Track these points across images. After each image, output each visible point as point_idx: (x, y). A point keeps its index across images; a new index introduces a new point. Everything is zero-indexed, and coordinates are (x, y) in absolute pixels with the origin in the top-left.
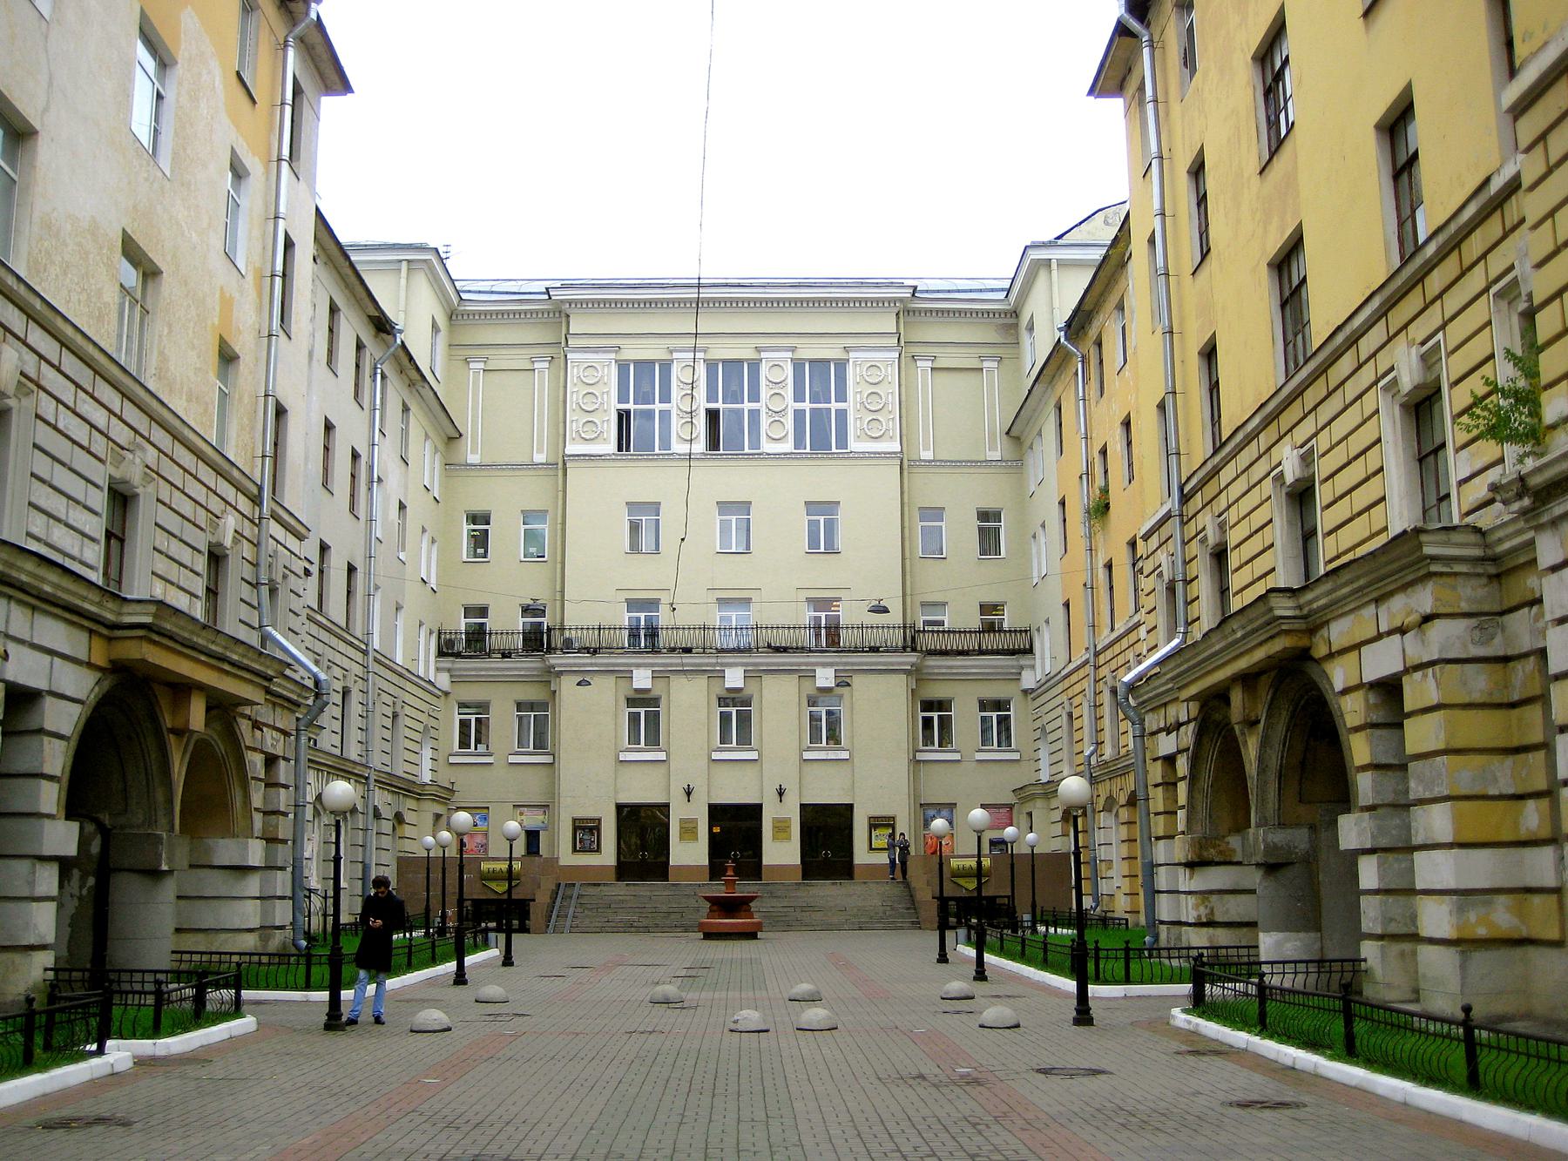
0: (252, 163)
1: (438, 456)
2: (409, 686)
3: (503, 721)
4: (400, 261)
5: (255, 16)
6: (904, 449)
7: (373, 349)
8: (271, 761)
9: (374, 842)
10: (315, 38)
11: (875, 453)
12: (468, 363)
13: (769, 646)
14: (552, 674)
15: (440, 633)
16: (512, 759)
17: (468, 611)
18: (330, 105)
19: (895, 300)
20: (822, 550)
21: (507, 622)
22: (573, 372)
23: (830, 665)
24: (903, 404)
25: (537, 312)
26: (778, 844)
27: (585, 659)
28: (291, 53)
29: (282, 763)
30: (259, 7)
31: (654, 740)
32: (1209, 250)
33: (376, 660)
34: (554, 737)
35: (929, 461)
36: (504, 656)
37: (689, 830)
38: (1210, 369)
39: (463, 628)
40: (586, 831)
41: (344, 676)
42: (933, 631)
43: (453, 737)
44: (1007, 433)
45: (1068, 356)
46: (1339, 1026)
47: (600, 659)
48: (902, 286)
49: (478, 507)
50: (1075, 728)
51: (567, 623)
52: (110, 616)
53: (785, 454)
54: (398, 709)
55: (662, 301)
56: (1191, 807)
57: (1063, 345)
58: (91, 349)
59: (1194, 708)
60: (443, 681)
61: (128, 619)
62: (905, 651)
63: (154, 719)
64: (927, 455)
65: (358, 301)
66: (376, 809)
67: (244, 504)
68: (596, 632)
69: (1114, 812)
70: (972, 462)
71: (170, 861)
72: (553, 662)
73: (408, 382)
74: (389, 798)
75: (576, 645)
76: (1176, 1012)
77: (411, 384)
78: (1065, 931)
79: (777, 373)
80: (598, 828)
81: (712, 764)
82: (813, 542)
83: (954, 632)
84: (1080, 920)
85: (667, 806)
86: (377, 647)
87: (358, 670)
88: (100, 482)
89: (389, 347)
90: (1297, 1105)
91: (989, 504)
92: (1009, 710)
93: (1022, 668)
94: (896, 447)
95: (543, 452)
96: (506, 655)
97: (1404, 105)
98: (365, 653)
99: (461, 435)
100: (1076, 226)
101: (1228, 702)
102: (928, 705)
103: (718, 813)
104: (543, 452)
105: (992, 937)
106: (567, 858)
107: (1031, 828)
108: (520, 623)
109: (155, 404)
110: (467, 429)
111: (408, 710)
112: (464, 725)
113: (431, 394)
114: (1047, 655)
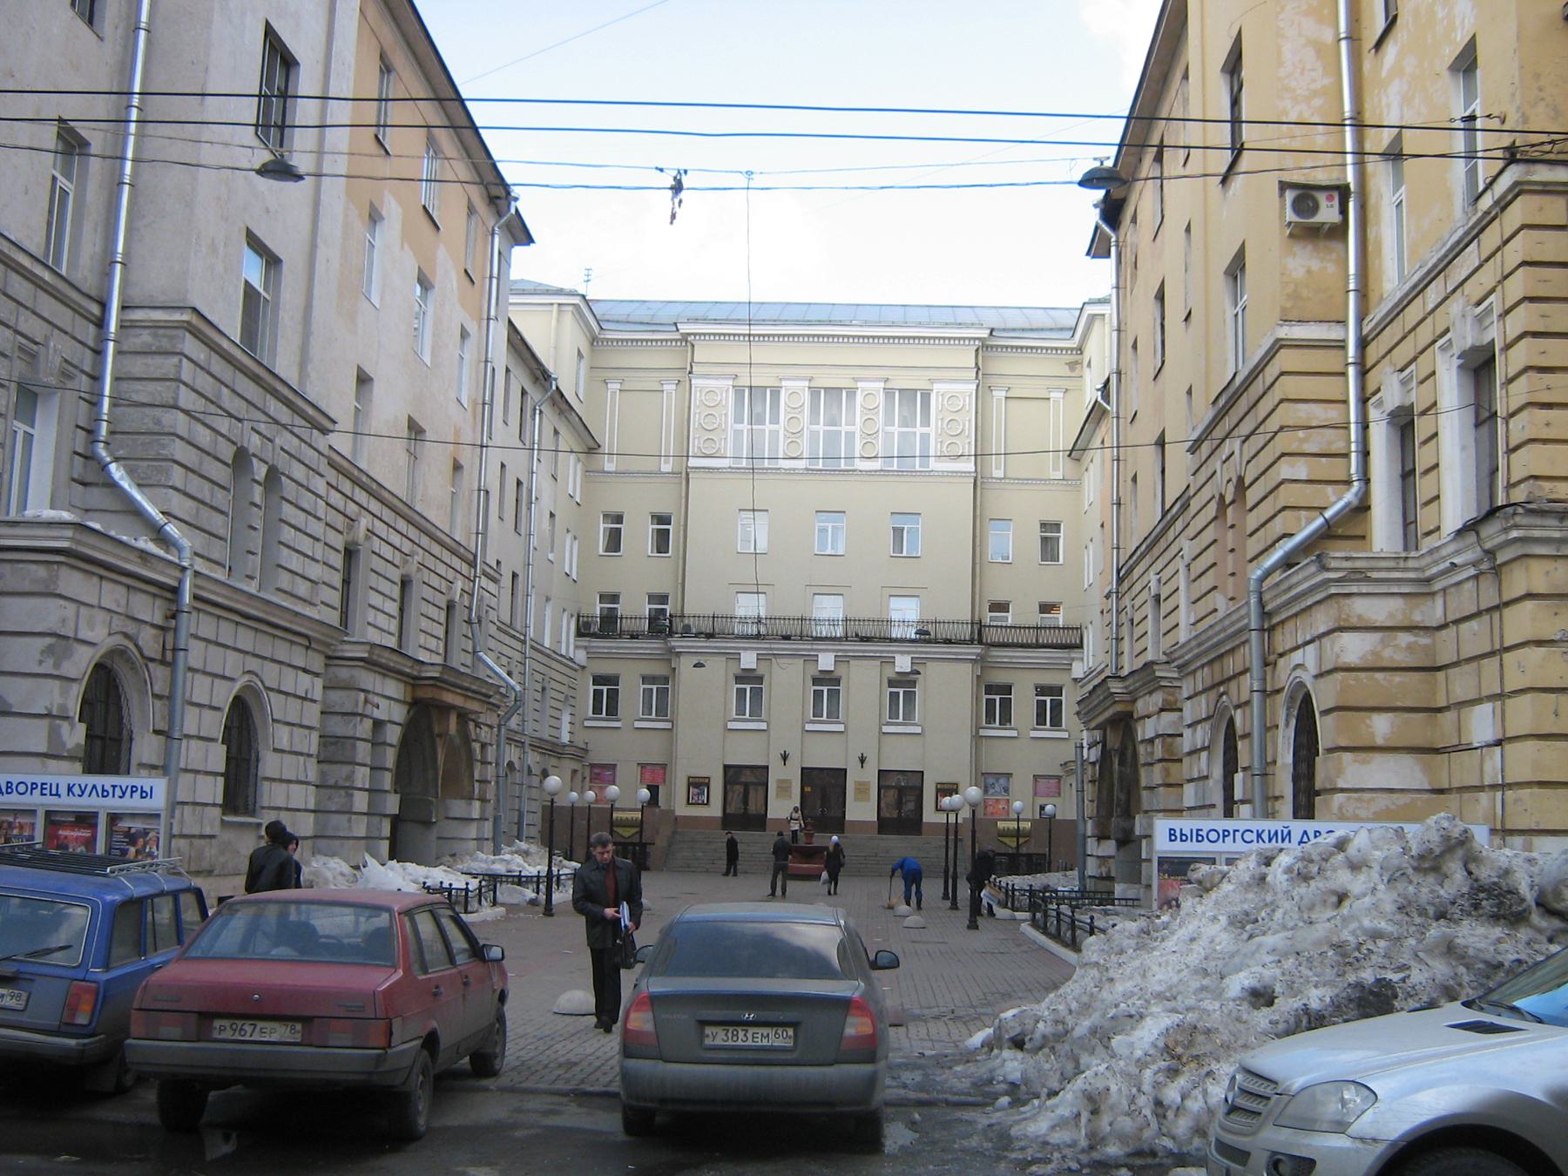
0: (472, 328)
1: (579, 466)
2: (554, 665)
3: (632, 693)
4: (552, 304)
5: (474, 218)
6: (979, 470)
7: (534, 394)
8: (484, 746)
9: (526, 794)
10: (516, 223)
11: (952, 472)
13: (857, 635)
14: (672, 654)
15: (579, 616)
16: (638, 724)
17: (603, 598)
18: (518, 252)
20: (904, 554)
21: (635, 607)
23: (908, 653)
27: (702, 643)
28: (497, 239)
29: (489, 748)
30: (477, 212)
31: (756, 712)
33: (532, 647)
34: (673, 706)
35: (1000, 479)
36: (632, 637)
39: (598, 613)
40: (698, 784)
41: (509, 663)
43: (588, 706)
45: (1104, 412)
47: (712, 643)
51: (686, 612)
52: (415, 673)
53: (876, 471)
54: (546, 685)
57: (1100, 403)
58: (396, 502)
60: (581, 656)
61: (424, 675)
62: (972, 644)
63: (430, 728)
65: (524, 361)
66: (529, 767)
67: (465, 568)
70: (1041, 480)
71: (436, 816)
72: (673, 644)
73: (558, 411)
74: (538, 758)
75: (694, 631)
77: (561, 412)
80: (708, 786)
81: (805, 734)
85: (767, 767)
86: (532, 635)
87: (517, 656)
89: (547, 391)
93: (1073, 659)
98: (524, 642)
102: (990, 689)
103: (807, 774)
106: (682, 810)
108: (646, 609)
109: (423, 522)
110: (607, 441)
111: (554, 685)
112: (598, 694)
113: (577, 419)
114: (1091, 653)
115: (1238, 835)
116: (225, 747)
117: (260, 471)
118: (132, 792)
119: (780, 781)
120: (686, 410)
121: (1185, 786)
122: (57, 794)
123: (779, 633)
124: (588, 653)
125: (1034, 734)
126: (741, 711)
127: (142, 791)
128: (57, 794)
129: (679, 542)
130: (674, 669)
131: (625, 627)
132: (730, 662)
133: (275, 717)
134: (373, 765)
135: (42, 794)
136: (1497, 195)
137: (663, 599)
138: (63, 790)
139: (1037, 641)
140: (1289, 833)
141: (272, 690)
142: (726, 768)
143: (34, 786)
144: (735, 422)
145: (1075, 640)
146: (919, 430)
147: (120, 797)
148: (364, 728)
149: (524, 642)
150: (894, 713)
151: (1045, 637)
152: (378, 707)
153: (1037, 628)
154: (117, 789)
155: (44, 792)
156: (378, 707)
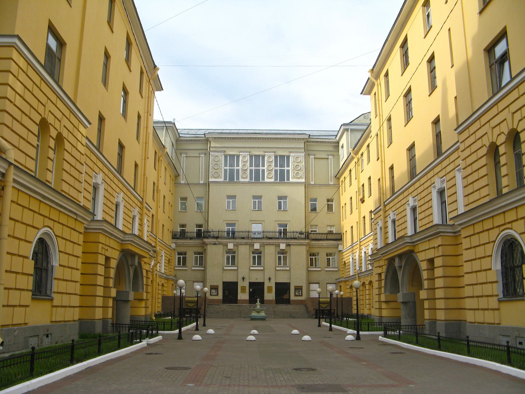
3: (191, 258)
6: (306, 182)
8: (147, 271)
12: (181, 154)
13: (267, 237)
15: (173, 232)
16: (193, 268)
19: (304, 139)
21: (192, 229)
22: (211, 158)
24: (306, 168)
25: (203, 140)
26: (269, 294)
27: (214, 240)
31: (259, 264)
32: (392, 142)
35: (313, 185)
37: (243, 289)
39: (179, 231)
42: (313, 234)
44: (336, 177)
46: (415, 338)
47: (220, 240)
48: (305, 134)
49: (184, 196)
55: (237, 138)
56: (385, 287)
59: (386, 262)
64: (312, 183)
68: (218, 233)
72: (205, 241)
76: (380, 337)
79: (269, 158)
82: (280, 207)
83: (319, 234)
84: (357, 316)
85: (237, 282)
88: (114, 203)
90: (405, 353)
94: (303, 180)
95: (202, 180)
96: (191, 238)
97: (437, 119)
99: (179, 175)
100: (356, 119)
101: (394, 261)
103: (251, 284)
104: (202, 180)
105: (333, 320)
107: (341, 290)
108: (195, 229)
112: (179, 258)
116: (33, 262)
117: (54, 133)
119: (242, 287)
120: (208, 163)
121: (435, 279)
123: (241, 236)
124: (176, 244)
126: (228, 263)
129: (206, 206)
130: (205, 249)
131: (188, 236)
132: (224, 247)
133: (61, 250)
134: (106, 276)
137: (200, 226)
139: (327, 238)
141: (59, 237)
142: (224, 283)
144: (225, 166)
146: (286, 168)
148: (101, 260)
149: (156, 239)
150: (280, 263)
151: (330, 237)
152: (107, 251)
153: (327, 234)
156: (107, 251)
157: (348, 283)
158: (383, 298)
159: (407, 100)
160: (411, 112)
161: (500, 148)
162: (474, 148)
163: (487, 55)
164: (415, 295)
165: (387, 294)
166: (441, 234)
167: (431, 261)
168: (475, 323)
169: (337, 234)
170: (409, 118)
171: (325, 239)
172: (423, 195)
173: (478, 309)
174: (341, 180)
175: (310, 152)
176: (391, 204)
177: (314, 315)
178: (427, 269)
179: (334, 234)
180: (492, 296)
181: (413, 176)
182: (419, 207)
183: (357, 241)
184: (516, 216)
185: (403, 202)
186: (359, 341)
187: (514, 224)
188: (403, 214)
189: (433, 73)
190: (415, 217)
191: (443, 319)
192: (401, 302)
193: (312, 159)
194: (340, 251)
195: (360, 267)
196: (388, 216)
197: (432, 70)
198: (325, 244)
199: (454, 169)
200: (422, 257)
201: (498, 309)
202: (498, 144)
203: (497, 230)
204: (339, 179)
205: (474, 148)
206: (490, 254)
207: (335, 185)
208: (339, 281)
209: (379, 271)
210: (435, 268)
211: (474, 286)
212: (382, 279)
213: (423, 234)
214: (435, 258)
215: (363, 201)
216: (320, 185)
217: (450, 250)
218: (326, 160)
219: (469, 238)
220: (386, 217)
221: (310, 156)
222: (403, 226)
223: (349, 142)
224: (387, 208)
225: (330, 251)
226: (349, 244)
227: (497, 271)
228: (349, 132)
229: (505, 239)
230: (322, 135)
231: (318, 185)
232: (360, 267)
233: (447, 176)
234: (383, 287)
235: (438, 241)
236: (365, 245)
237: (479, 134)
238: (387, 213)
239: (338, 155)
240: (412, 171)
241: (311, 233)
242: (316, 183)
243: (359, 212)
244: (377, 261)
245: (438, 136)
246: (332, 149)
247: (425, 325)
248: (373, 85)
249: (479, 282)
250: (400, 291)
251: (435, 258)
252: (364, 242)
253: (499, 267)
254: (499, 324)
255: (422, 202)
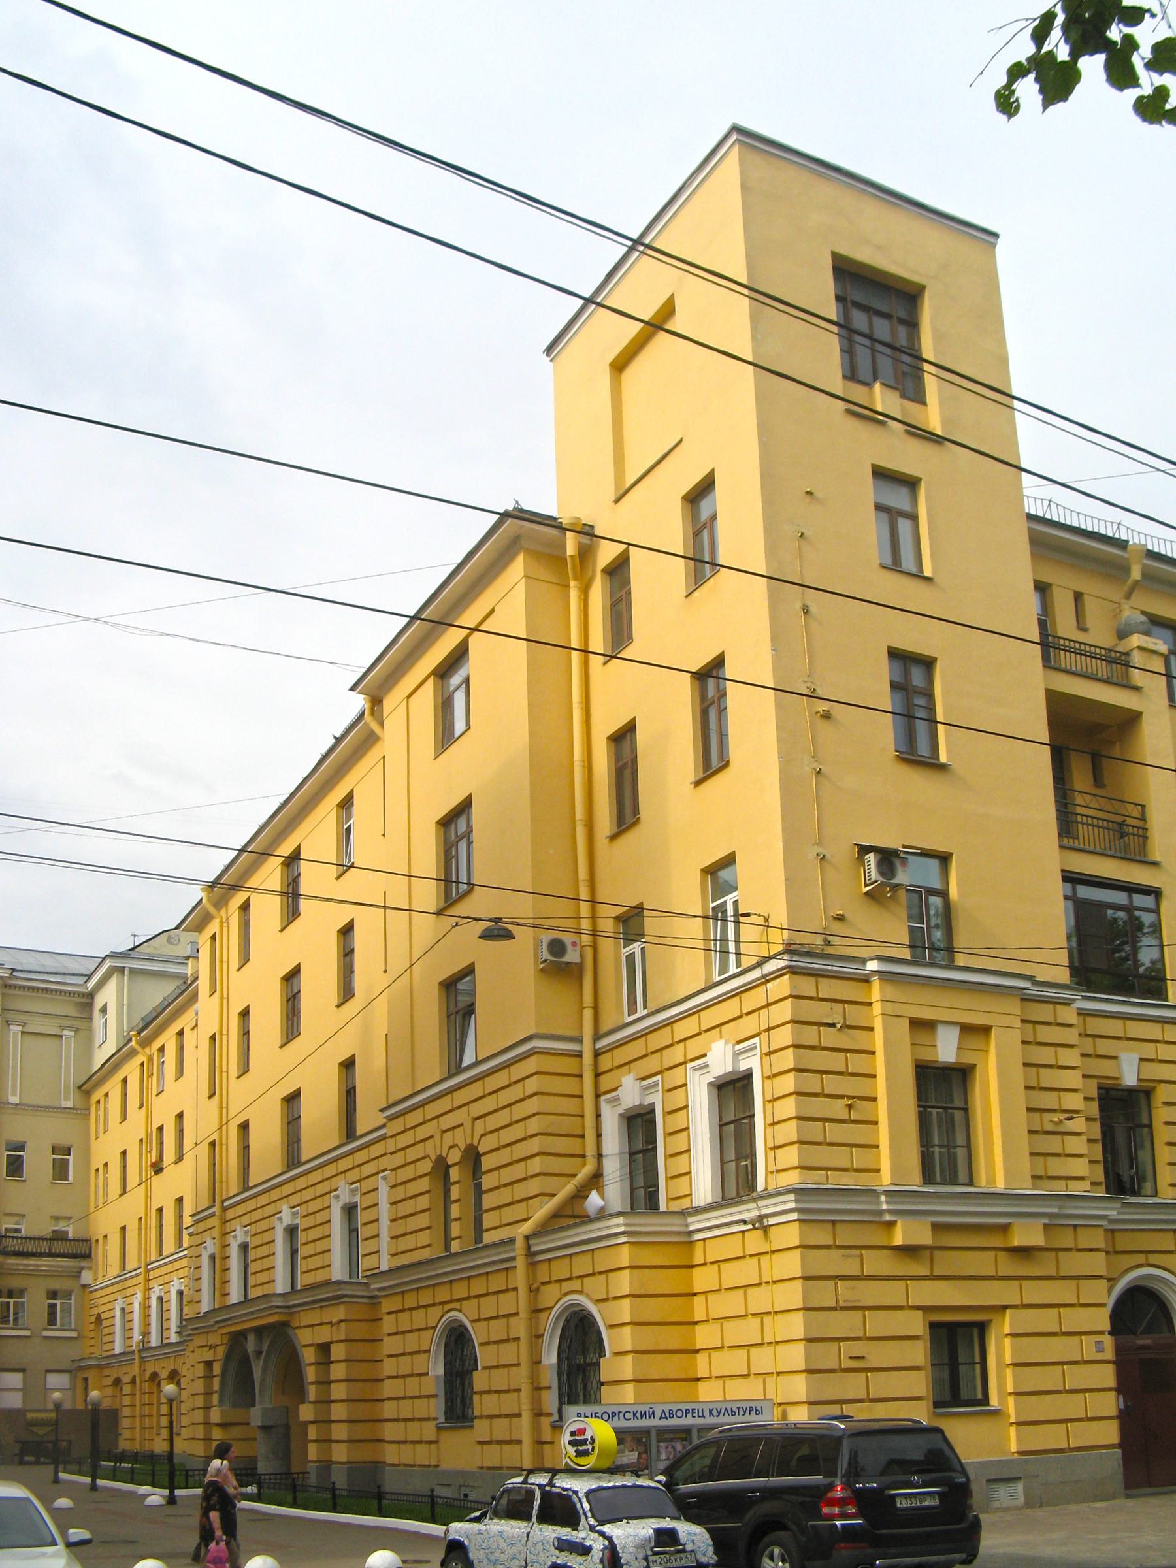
35: (17, 1105)
38: (244, 1135)
42: (13, 1237)
44: (80, 1087)
50: (127, 1320)
56: (222, 1392)
64: (14, 1100)
69: (157, 1381)
78: (126, 1465)
91: (63, 1141)
92: (70, 1299)
93: (82, 1268)
101: (246, 1338)
115: (621, 1415)
118: (750, 1411)
122: (703, 1416)
125: (46, 1333)
127: (756, 1410)
128: (703, 1416)
135: (693, 1417)
136: (765, 972)
138: (706, 1413)
139: (50, 1249)
140: (653, 1411)
143: (687, 1411)
145: (85, 1251)
147: (743, 1415)
151: (58, 1247)
154: (741, 1410)
155: (694, 1415)
157: (106, 1372)
158: (215, 1416)
159: (290, 990)
160: (295, 1018)
161: (451, 1170)
162: (412, 1154)
163: (444, 992)
164: (289, 1413)
165: (225, 1408)
166: (345, 1299)
167: (324, 1348)
168: (399, 1465)
169: (78, 1240)
170: (290, 1032)
171: (45, 1253)
172: (313, 1206)
173: (405, 1442)
174: (94, 1098)
175: (10, 1016)
176: (240, 1210)
177: (15, 1455)
178: (317, 1363)
179: (70, 1240)
180: (428, 1419)
181: (293, 1161)
182: (305, 1230)
183: (140, 1268)
184: (467, 1292)
185: (269, 1210)
186: (174, 1506)
187: (464, 1303)
188: (267, 1237)
189: (348, 958)
190: (294, 1247)
191: (345, 1460)
192: (259, 1427)
193: (15, 1034)
194: (84, 1286)
195: (146, 1334)
196: (230, 1233)
197: (347, 954)
198: (45, 1266)
199: (377, 1173)
200: (306, 1338)
201: (436, 1442)
202: (450, 1163)
203: (438, 1310)
204: (88, 1094)
205: (412, 1154)
206: (428, 1349)
207: (77, 1109)
208: (81, 1367)
209: (208, 1355)
210: (332, 1362)
211: (401, 1401)
212: (214, 1374)
213: (310, 1294)
214: (332, 1342)
215: (158, 1168)
216: (33, 1106)
217: (360, 1331)
218: (55, 1041)
219: (394, 1315)
220: (228, 1233)
221: (12, 1027)
222: (266, 1263)
223: (125, 1002)
224: (230, 1214)
225: (56, 1284)
226: (114, 1270)
227: (437, 1377)
228: (126, 978)
229: (449, 1328)
230: (48, 970)
231: (29, 1106)
232: (146, 1334)
233: (362, 1182)
234: (216, 1392)
235: (339, 1313)
236: (161, 1280)
237: (421, 1133)
238: (229, 1228)
239: (90, 1030)
240: (290, 1147)
241: (5, 1237)
242: (25, 1101)
243: (147, 1195)
244: (203, 1333)
245: (350, 1094)
246: (72, 1011)
247: (309, 1473)
248: (206, 919)
249: (408, 1394)
250: (257, 1404)
251: (332, 1342)
252: (157, 1273)
253: (440, 1371)
254: (437, 1466)
255: (310, 1221)
